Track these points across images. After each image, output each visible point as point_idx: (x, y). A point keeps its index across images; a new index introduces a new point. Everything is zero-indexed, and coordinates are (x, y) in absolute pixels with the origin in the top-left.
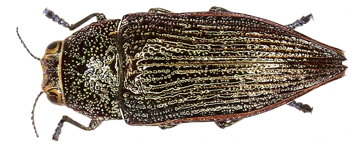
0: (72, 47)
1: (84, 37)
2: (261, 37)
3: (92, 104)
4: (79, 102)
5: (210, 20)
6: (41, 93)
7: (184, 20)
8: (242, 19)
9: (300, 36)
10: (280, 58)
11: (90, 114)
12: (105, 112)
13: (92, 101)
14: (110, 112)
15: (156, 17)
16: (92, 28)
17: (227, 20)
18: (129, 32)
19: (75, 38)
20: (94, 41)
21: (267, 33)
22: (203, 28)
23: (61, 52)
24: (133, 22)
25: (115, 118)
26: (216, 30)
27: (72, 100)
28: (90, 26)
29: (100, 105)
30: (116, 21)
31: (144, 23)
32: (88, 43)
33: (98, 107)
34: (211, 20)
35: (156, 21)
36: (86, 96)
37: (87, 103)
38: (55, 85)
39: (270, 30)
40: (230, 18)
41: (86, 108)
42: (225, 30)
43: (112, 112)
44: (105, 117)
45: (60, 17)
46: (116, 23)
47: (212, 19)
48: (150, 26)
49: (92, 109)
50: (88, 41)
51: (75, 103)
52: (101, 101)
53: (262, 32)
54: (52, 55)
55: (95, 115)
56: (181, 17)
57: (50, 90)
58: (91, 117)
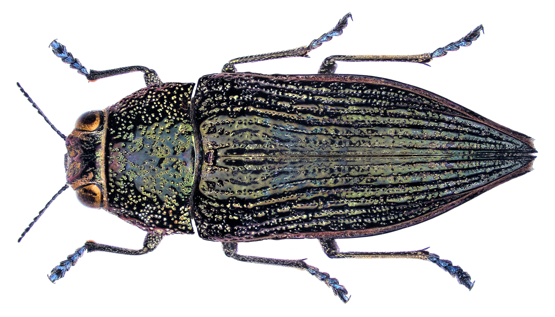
0: (121, 122)
1: (141, 108)
2: (409, 117)
3: (150, 211)
4: (130, 207)
5: (334, 89)
6: (64, 188)
7: (295, 88)
8: (382, 89)
9: (468, 115)
10: (437, 149)
11: (145, 225)
12: (169, 221)
13: (151, 206)
14: (176, 222)
15: (253, 81)
16: (151, 95)
17: (360, 89)
18: (210, 105)
19: (125, 108)
20: (155, 117)
21: (419, 110)
22: (323, 102)
23: (104, 129)
24: (215, 89)
25: (184, 231)
26: (343, 105)
27: (118, 203)
28: (148, 92)
29: (162, 212)
30: (189, 85)
31: (232, 92)
32: (146, 119)
33: (158, 215)
34: (335, 88)
35: (254, 88)
36: (141, 198)
37: (143, 208)
38: (94, 179)
39: (423, 107)
40: (364, 86)
41: (140, 215)
42: (357, 105)
43: (179, 223)
44: (168, 230)
45: (75, 57)
46: (189, 89)
47: (338, 87)
48: (241, 98)
49: (149, 217)
50: (147, 115)
51: (124, 207)
52: (164, 206)
53: (411, 109)
54: (89, 133)
55: (152, 227)
56: (290, 83)
57: (84, 186)
58: (144, 228)
